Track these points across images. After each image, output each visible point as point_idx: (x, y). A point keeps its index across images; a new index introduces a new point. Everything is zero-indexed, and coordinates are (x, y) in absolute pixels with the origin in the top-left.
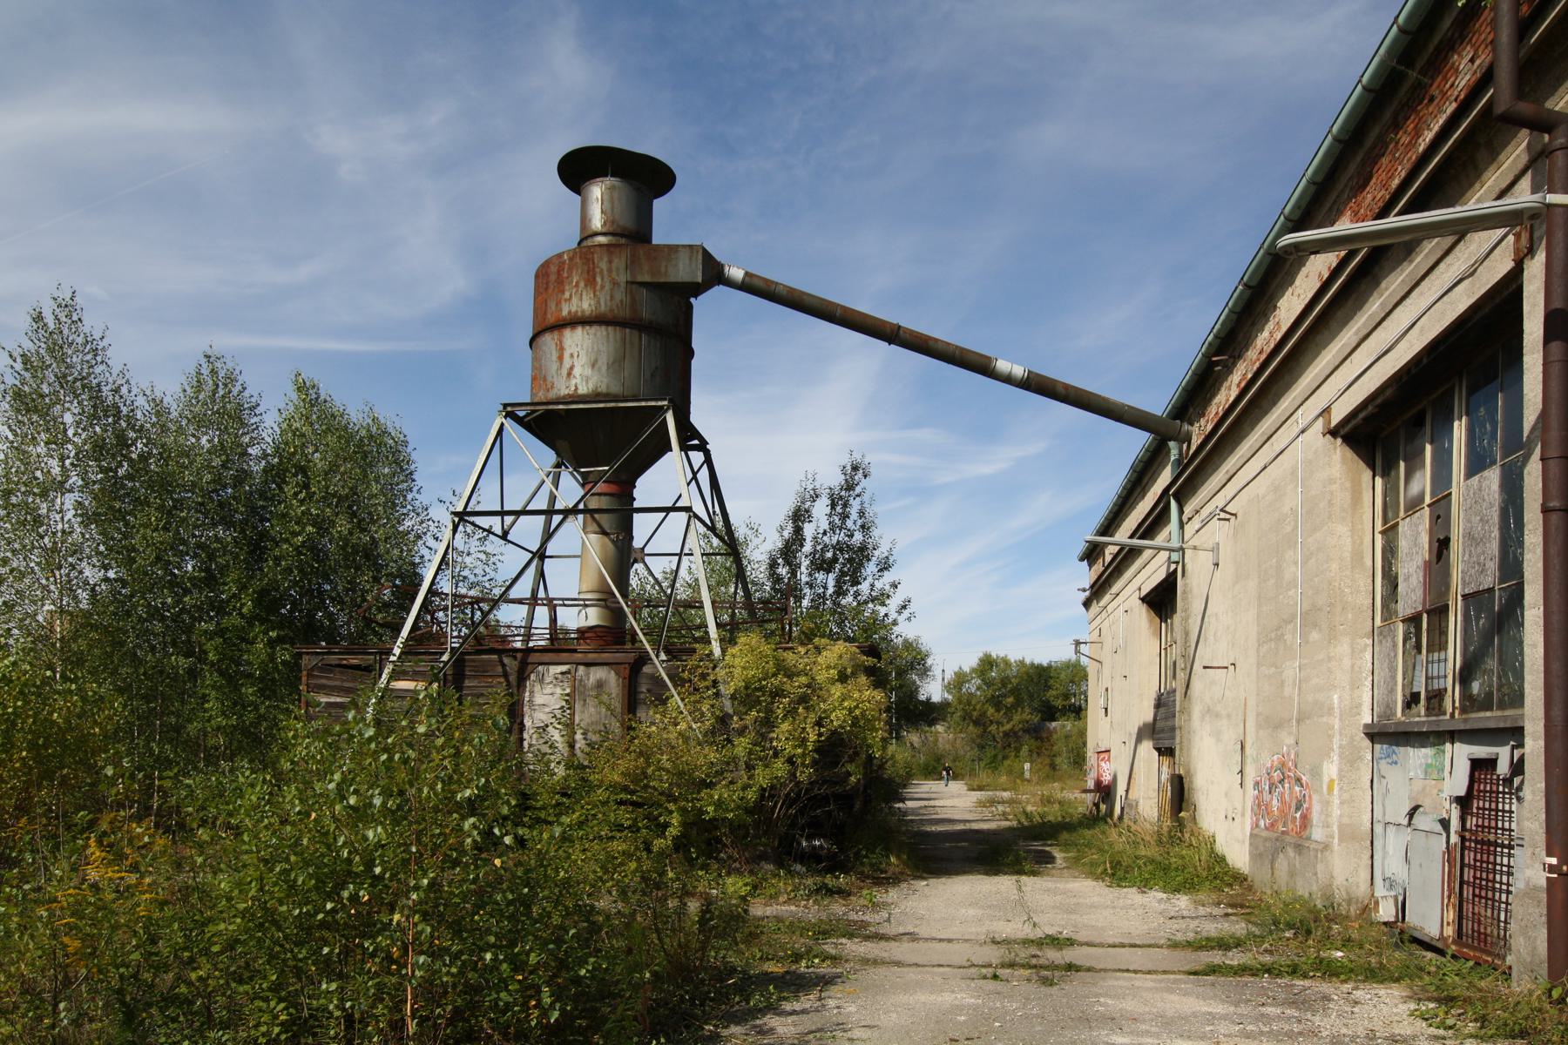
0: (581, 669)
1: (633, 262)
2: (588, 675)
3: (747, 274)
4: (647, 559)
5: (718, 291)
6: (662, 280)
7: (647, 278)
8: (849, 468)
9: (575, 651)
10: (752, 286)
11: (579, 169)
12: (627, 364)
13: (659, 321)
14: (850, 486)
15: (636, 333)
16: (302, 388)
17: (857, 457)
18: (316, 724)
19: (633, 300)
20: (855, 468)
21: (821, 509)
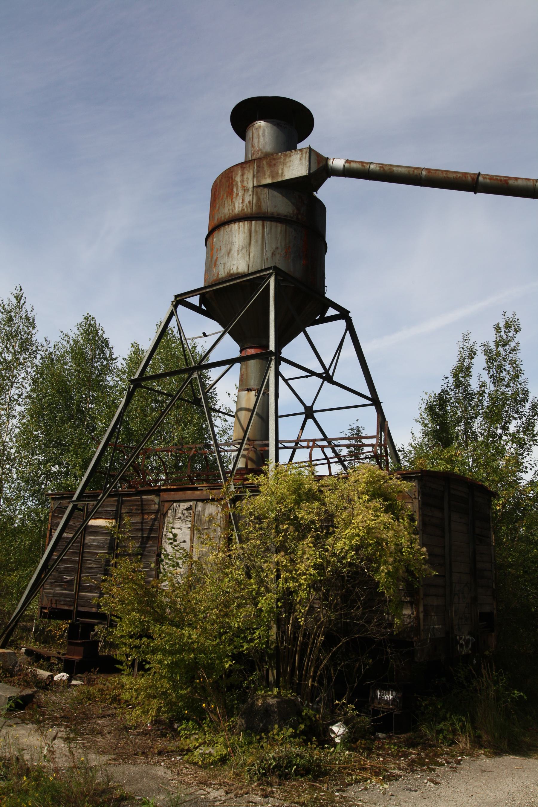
0: (200, 504)
1: (258, 171)
2: (204, 509)
3: (347, 161)
4: (315, 415)
5: (331, 182)
6: (280, 179)
7: (269, 181)
8: (502, 325)
9: (196, 489)
10: (347, 172)
11: (244, 116)
12: (253, 248)
13: (299, 220)
14: (501, 343)
15: (260, 223)
16: (87, 319)
17: (509, 315)
18: (254, 593)
19: (259, 199)
20: (508, 326)
21: (479, 363)
